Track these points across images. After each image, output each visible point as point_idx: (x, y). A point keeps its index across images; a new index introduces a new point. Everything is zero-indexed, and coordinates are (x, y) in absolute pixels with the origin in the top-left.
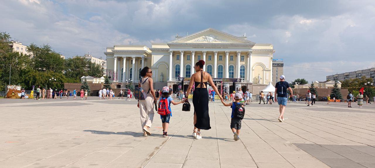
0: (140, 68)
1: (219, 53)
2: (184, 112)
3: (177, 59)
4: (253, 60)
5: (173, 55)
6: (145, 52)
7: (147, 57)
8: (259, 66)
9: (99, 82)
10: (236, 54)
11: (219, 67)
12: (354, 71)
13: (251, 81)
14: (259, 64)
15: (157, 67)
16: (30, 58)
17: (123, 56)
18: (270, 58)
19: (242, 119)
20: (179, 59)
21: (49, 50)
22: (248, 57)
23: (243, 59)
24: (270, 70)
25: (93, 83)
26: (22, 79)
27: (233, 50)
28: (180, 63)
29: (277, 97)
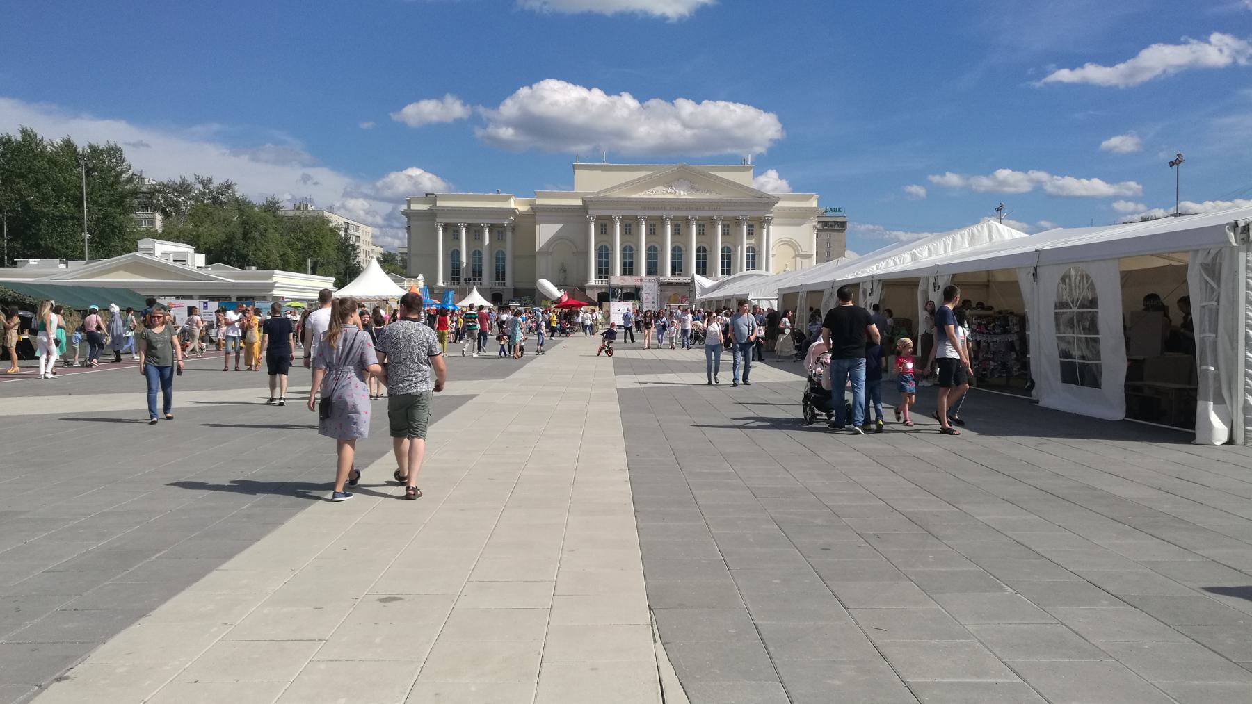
1: (649, 219)
5: (467, 232)
8: (785, 246)
15: (550, 250)
16: (859, 227)
17: (664, 214)
20: (479, 239)
21: (279, 208)
24: (810, 256)
27: (706, 214)
28: (459, 245)
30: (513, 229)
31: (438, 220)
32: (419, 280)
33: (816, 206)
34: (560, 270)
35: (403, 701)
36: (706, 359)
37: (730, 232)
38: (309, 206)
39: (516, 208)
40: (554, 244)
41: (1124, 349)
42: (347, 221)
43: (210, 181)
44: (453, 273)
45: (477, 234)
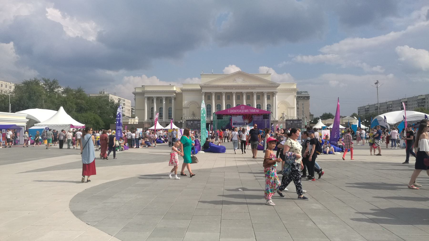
0: (151, 107)
2: (96, 174)
3: (258, 99)
4: (277, 100)
6: (174, 92)
7: (176, 96)
9: (134, 122)
10: (262, 94)
11: (218, 106)
12: (397, 99)
13: (277, 119)
14: (189, 104)
18: (294, 96)
19: (409, 160)
22: (273, 96)
23: (248, 98)
25: (129, 123)
26: (76, 95)
28: (212, 103)
29: (414, 123)
30: (175, 99)
31: (145, 96)
32: (135, 119)
33: (296, 88)
34: (192, 114)
35: (145, 240)
36: (113, 154)
37: (260, 98)
38: (105, 92)
39: (176, 91)
40: (190, 104)
41: (33, 161)
42: (120, 98)
43: (49, 80)
44: (169, 116)
45: (170, 101)
